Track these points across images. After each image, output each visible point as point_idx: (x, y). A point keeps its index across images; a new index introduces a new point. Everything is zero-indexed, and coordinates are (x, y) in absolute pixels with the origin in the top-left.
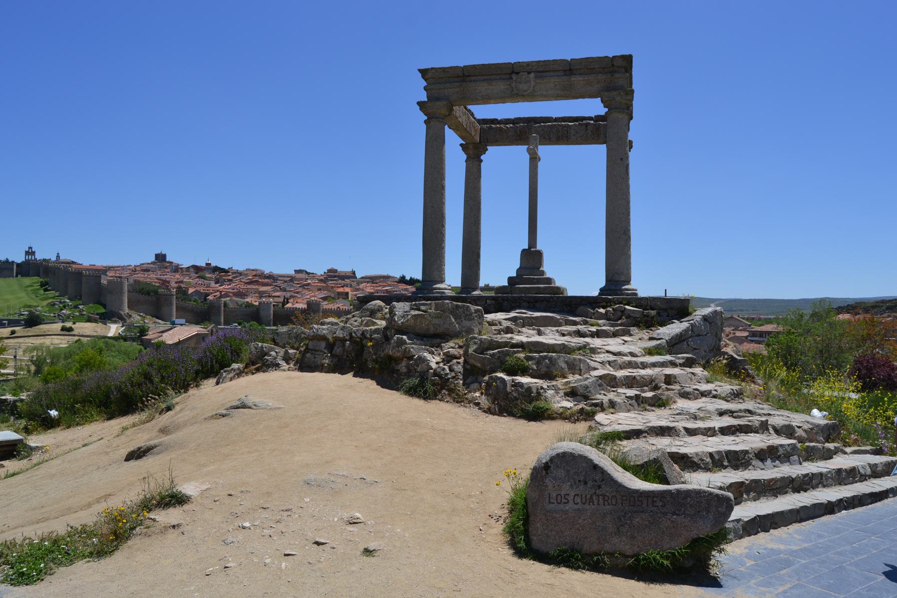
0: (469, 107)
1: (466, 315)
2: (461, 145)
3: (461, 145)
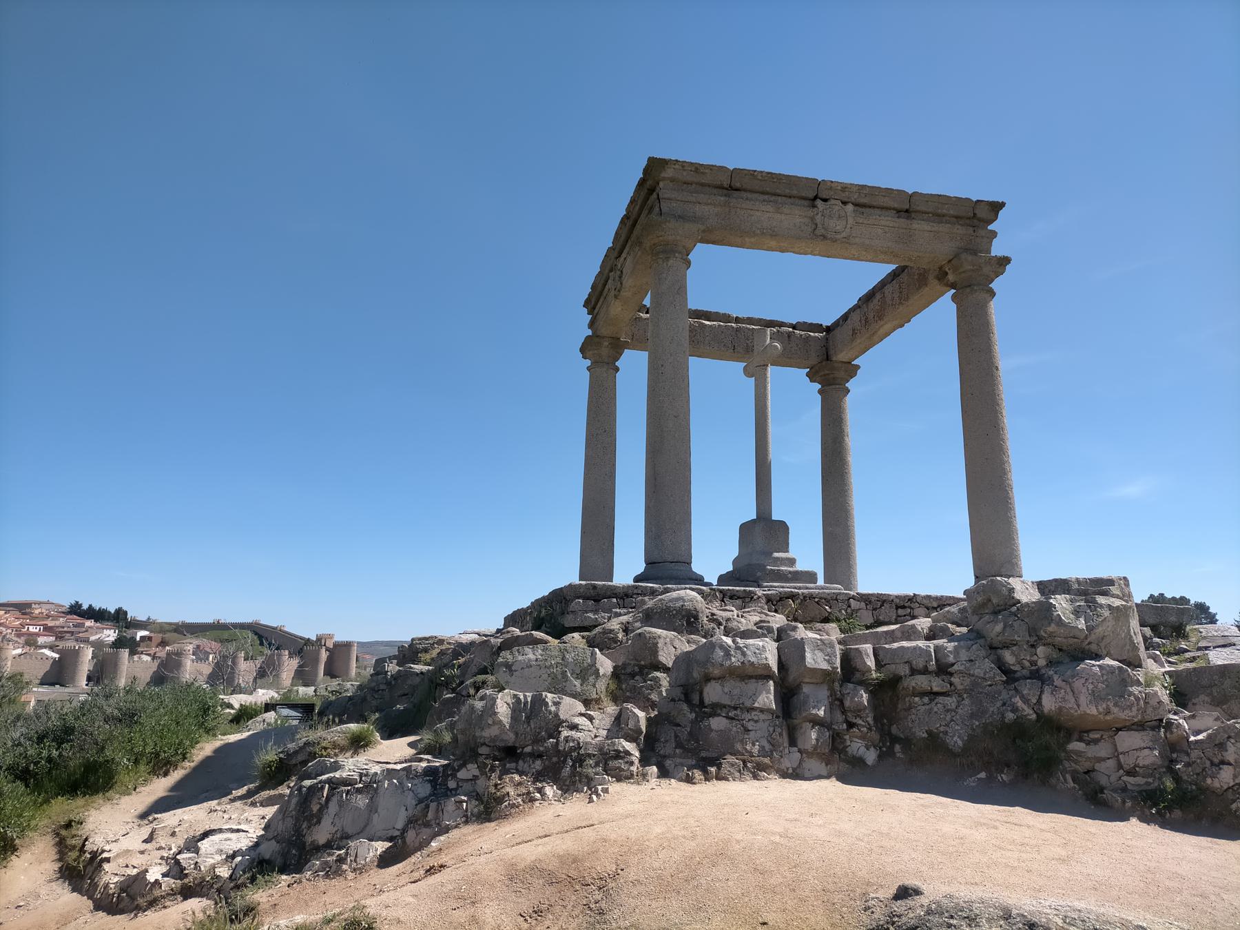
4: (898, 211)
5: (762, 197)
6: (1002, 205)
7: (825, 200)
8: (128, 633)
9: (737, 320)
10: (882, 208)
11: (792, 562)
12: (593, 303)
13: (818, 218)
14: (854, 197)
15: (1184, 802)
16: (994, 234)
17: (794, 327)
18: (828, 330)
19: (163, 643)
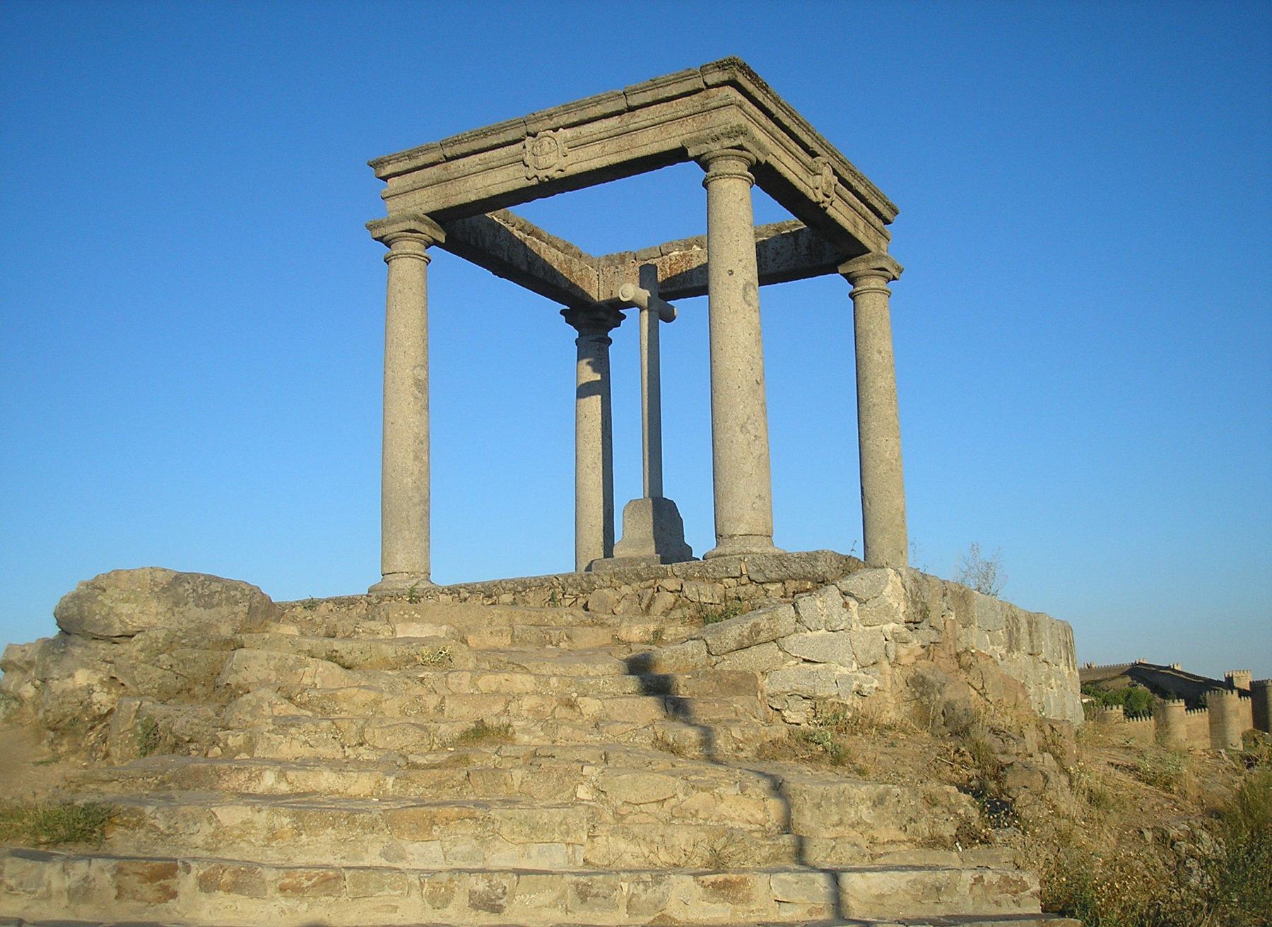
1: (201, 596)
2: (562, 312)
3: (562, 312)
7: (535, 135)
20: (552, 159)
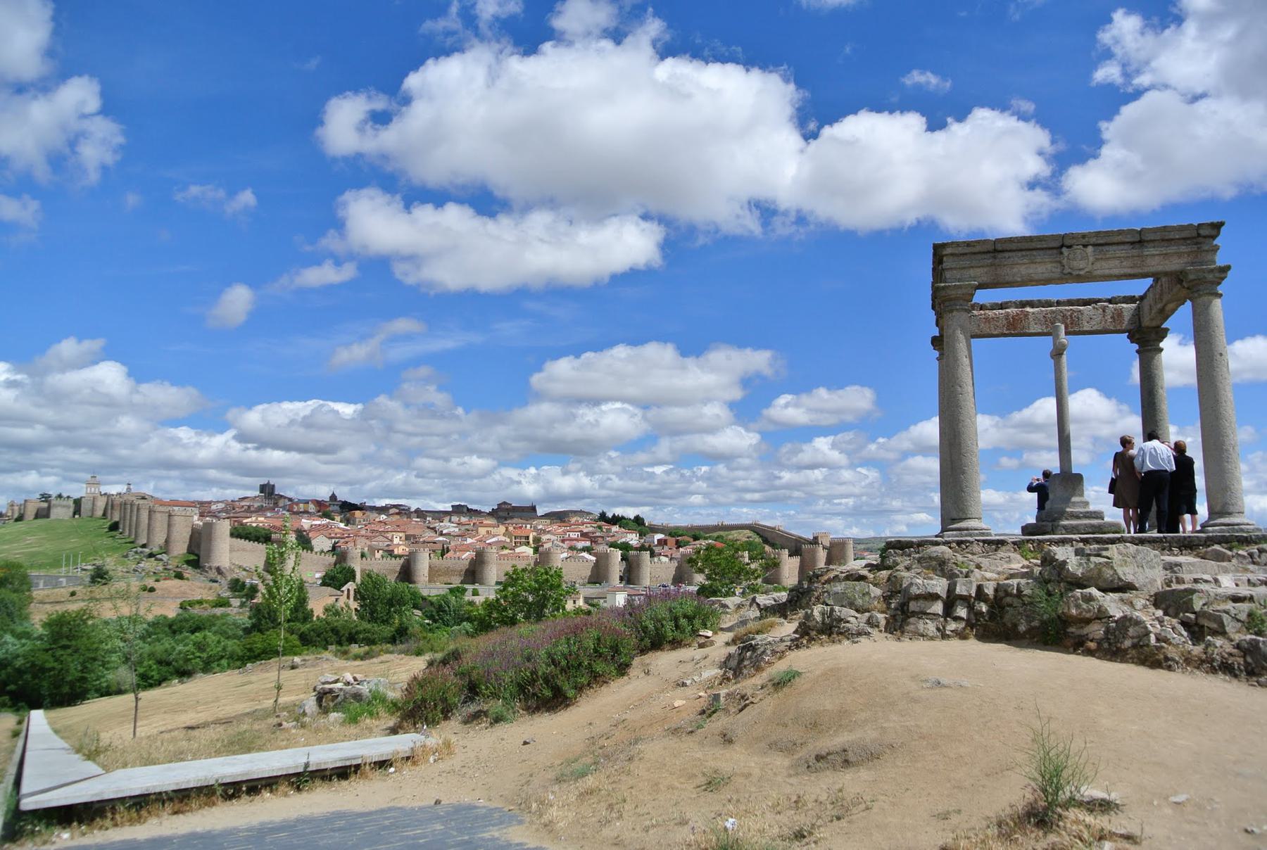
0: (1150, 281)
4: (1132, 243)
5: (1020, 254)
6: (1222, 224)
7: (1069, 247)
8: (647, 538)
9: (1059, 303)
10: (1118, 244)
11: (1087, 503)
12: (933, 308)
13: (1065, 261)
14: (1093, 240)
15: (1255, 665)
16: (1216, 248)
17: (1110, 301)
18: (1142, 298)
19: (679, 545)
20: (1082, 264)
